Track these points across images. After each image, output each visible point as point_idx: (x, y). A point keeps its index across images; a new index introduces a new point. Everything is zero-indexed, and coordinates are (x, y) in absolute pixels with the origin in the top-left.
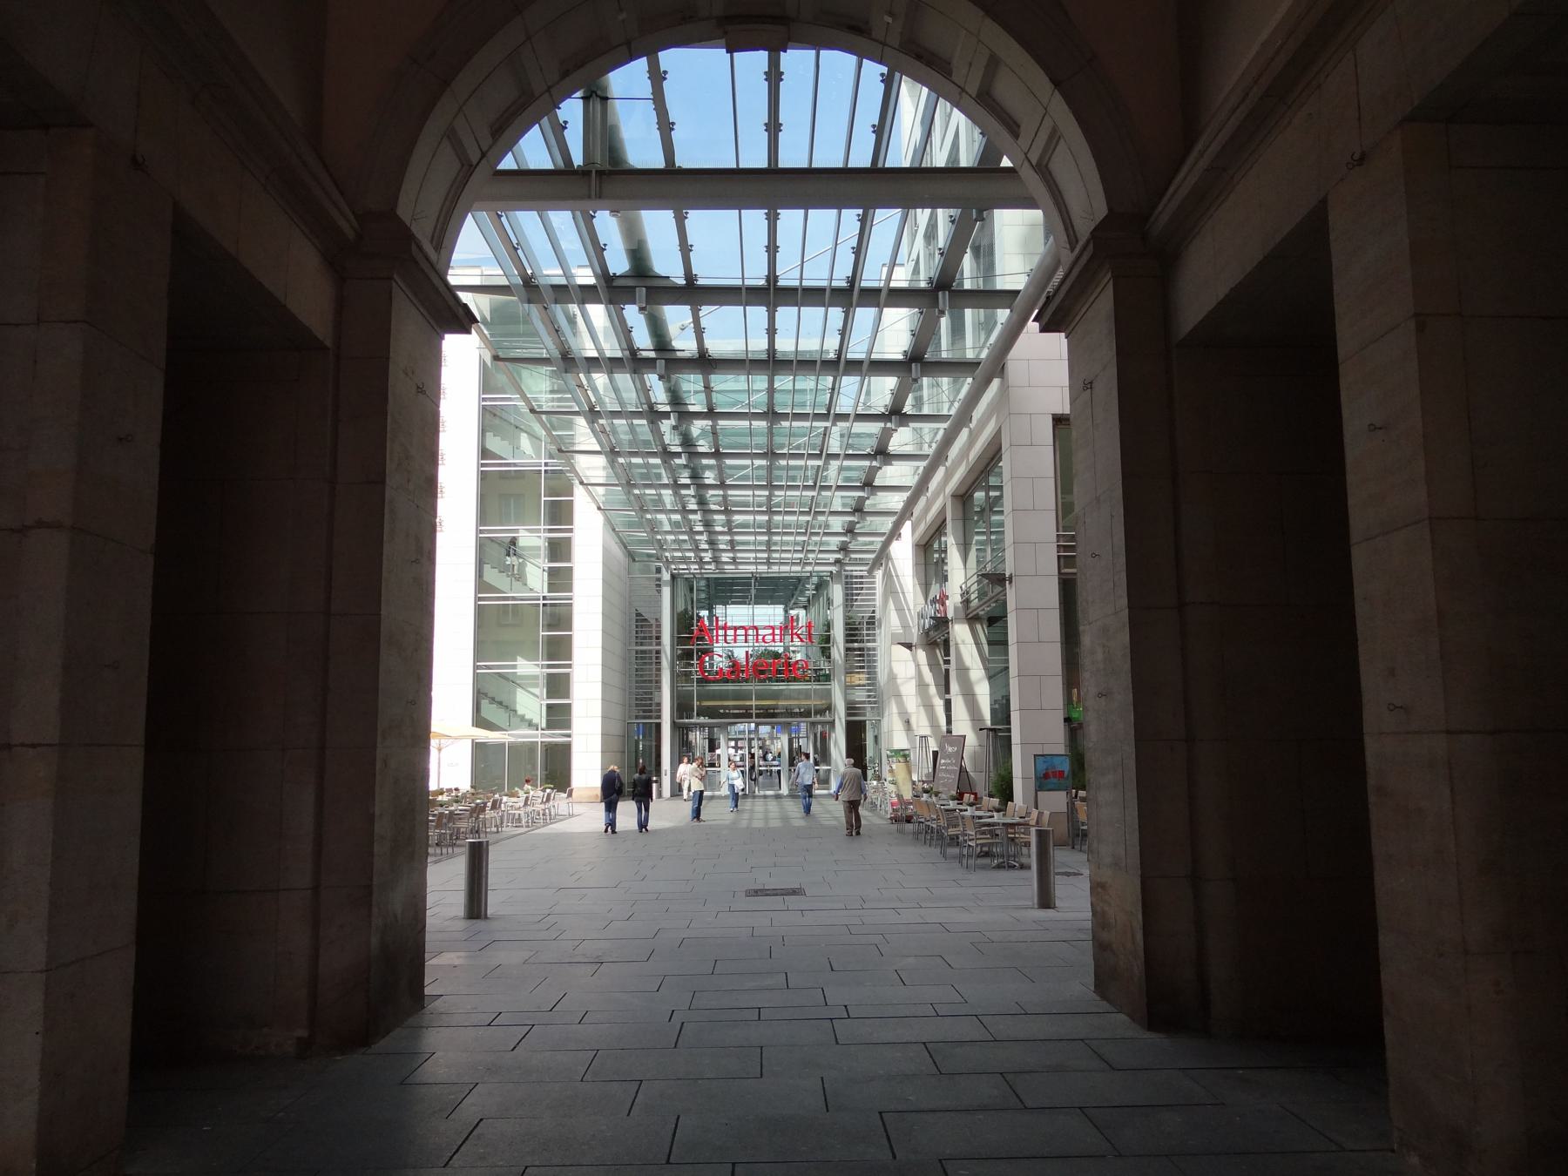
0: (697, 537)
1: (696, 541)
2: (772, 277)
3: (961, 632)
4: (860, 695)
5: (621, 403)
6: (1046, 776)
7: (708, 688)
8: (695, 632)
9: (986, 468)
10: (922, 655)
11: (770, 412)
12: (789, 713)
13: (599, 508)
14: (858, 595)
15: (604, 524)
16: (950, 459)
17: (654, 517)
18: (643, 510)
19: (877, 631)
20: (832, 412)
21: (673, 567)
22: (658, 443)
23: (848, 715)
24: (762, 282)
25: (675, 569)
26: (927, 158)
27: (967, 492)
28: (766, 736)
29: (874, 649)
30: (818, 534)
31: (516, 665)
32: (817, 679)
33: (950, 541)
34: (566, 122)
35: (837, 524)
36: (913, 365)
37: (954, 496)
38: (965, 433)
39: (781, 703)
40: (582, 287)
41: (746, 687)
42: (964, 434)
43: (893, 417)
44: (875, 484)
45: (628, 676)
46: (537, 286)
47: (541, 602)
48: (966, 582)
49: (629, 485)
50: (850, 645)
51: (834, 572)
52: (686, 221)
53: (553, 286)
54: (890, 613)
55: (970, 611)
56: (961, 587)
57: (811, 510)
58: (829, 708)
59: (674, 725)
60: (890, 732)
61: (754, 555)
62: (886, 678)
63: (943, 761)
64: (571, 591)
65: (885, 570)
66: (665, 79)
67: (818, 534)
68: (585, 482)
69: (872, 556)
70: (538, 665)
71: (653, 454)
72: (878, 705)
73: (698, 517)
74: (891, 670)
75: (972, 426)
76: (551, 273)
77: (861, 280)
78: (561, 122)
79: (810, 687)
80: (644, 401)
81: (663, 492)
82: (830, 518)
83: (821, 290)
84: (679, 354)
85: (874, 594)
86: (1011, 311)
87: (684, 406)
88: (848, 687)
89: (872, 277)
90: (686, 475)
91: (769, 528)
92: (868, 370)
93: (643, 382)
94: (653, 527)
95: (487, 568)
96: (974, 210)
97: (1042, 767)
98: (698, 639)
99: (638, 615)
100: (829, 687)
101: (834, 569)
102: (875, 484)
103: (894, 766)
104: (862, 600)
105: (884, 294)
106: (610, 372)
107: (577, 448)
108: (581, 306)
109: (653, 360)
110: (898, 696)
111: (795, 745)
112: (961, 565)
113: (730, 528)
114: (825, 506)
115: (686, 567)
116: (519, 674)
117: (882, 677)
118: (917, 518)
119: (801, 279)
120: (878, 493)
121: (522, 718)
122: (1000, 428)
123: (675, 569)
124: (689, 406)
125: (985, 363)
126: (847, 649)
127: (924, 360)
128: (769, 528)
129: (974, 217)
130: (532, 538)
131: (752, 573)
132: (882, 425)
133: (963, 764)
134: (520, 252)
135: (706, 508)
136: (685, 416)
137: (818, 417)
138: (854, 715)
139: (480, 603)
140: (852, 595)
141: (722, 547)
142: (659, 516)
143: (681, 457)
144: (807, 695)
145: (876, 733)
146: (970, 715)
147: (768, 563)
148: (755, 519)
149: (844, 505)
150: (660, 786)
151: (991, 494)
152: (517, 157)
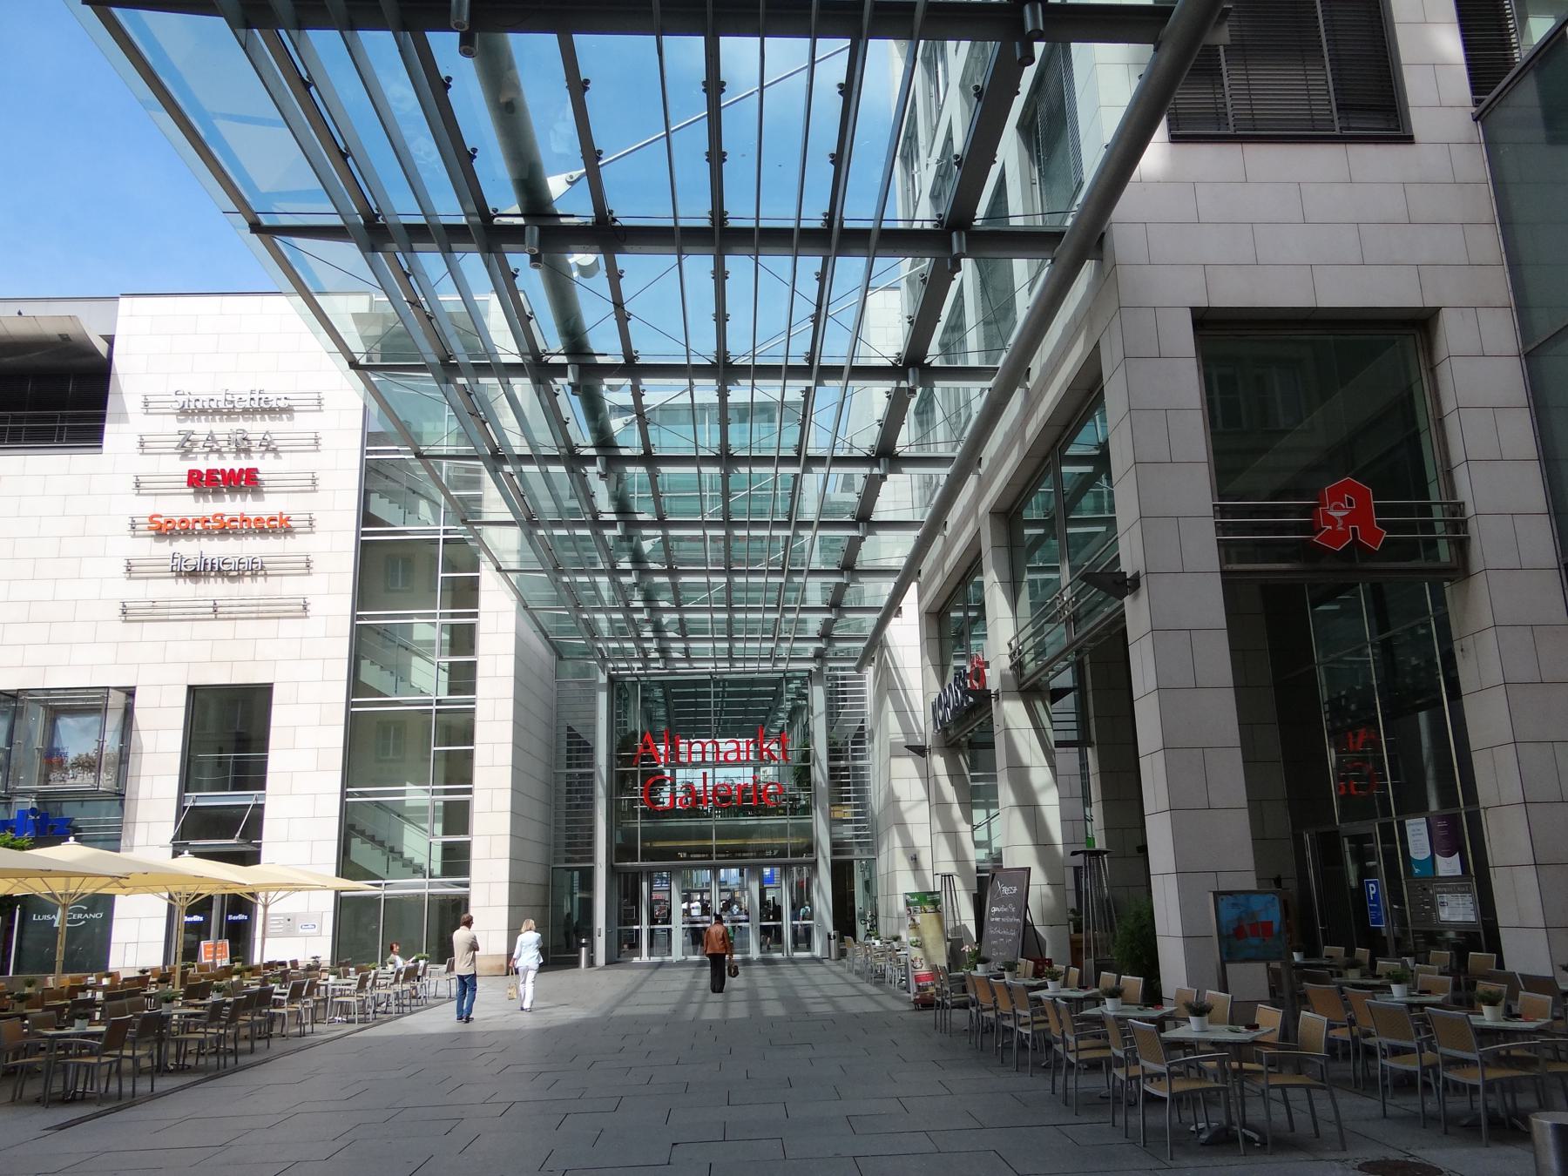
0: (646, 645)
1: (643, 649)
2: (718, 212)
3: (1013, 713)
4: (847, 832)
5: (532, 445)
6: (1239, 932)
7: (657, 825)
8: (640, 748)
9: (1053, 446)
10: (939, 763)
11: (721, 366)
12: (760, 852)
13: (354, 365)
14: (845, 700)
15: (517, 609)
16: (949, 526)
17: (573, 580)
18: (578, 607)
19: (868, 746)
20: (816, 364)
21: (611, 665)
22: (587, 510)
23: (834, 853)
24: (706, 223)
25: (614, 669)
26: (862, 349)
27: (1012, 506)
28: (736, 887)
29: (862, 768)
30: (787, 639)
31: (404, 791)
32: (794, 811)
33: (992, 584)
34: (475, 150)
35: (814, 623)
36: (911, 370)
37: (995, 513)
38: (972, 481)
39: (750, 842)
40: (447, 227)
41: (705, 823)
42: (972, 482)
43: (882, 460)
44: (874, 518)
45: (553, 807)
46: (384, 226)
47: (434, 707)
48: (1017, 636)
49: (557, 570)
50: (835, 764)
51: (814, 670)
52: (621, 280)
53: (407, 226)
54: (887, 714)
55: (1024, 679)
56: (1010, 645)
57: (778, 605)
58: (810, 849)
59: (612, 871)
60: (891, 874)
61: (713, 665)
62: (882, 801)
63: (995, 909)
64: (474, 693)
65: (880, 662)
66: (621, 277)
67: (787, 639)
68: (503, 568)
69: (862, 645)
70: (427, 790)
71: (582, 524)
72: (871, 844)
73: (654, 645)
74: (890, 791)
75: (1029, 384)
76: (403, 208)
77: (820, 356)
78: (469, 149)
79: (785, 821)
80: (563, 444)
81: (598, 579)
82: (809, 579)
83: (787, 233)
84: (600, 360)
85: (863, 699)
86: (1156, 50)
87: (591, 358)
88: (834, 822)
89: (858, 213)
90: (649, 628)
91: (729, 601)
92: (879, 246)
93: (504, 265)
94: (591, 629)
95: (365, 664)
96: (1017, 43)
97: (1230, 914)
98: (644, 759)
99: (570, 729)
100: (810, 821)
101: (811, 666)
102: (874, 518)
103: (918, 919)
104: (851, 707)
105: (874, 237)
106: (447, 251)
107: (486, 518)
108: (347, 33)
109: (519, 229)
110: (901, 824)
111: (769, 897)
112: (1009, 613)
113: (683, 629)
114: (803, 565)
115: (626, 665)
116: (407, 804)
117: (876, 799)
118: (927, 575)
119: (758, 219)
120: (878, 532)
121: (408, 863)
122: (1097, 346)
123: (614, 669)
124: (597, 358)
125: (1070, 233)
126: (831, 769)
127: (973, 229)
128: (729, 601)
129: (1018, 56)
130: (428, 626)
131: (710, 673)
132: (893, 384)
133: (1028, 917)
134: (488, 425)
135: (644, 567)
136: (589, 373)
137: (785, 461)
138: (843, 853)
139: (353, 710)
140: (838, 700)
141: (675, 655)
142: (600, 616)
143: (615, 528)
144: (782, 831)
145: (867, 877)
146: (1033, 840)
147: (731, 659)
148: (709, 581)
149: (825, 562)
150: (591, 950)
151: (971, 614)
152: (376, 102)
